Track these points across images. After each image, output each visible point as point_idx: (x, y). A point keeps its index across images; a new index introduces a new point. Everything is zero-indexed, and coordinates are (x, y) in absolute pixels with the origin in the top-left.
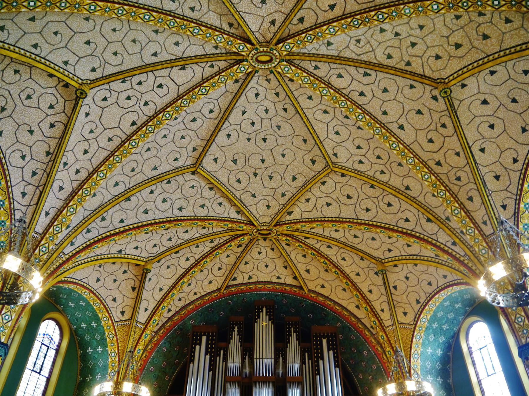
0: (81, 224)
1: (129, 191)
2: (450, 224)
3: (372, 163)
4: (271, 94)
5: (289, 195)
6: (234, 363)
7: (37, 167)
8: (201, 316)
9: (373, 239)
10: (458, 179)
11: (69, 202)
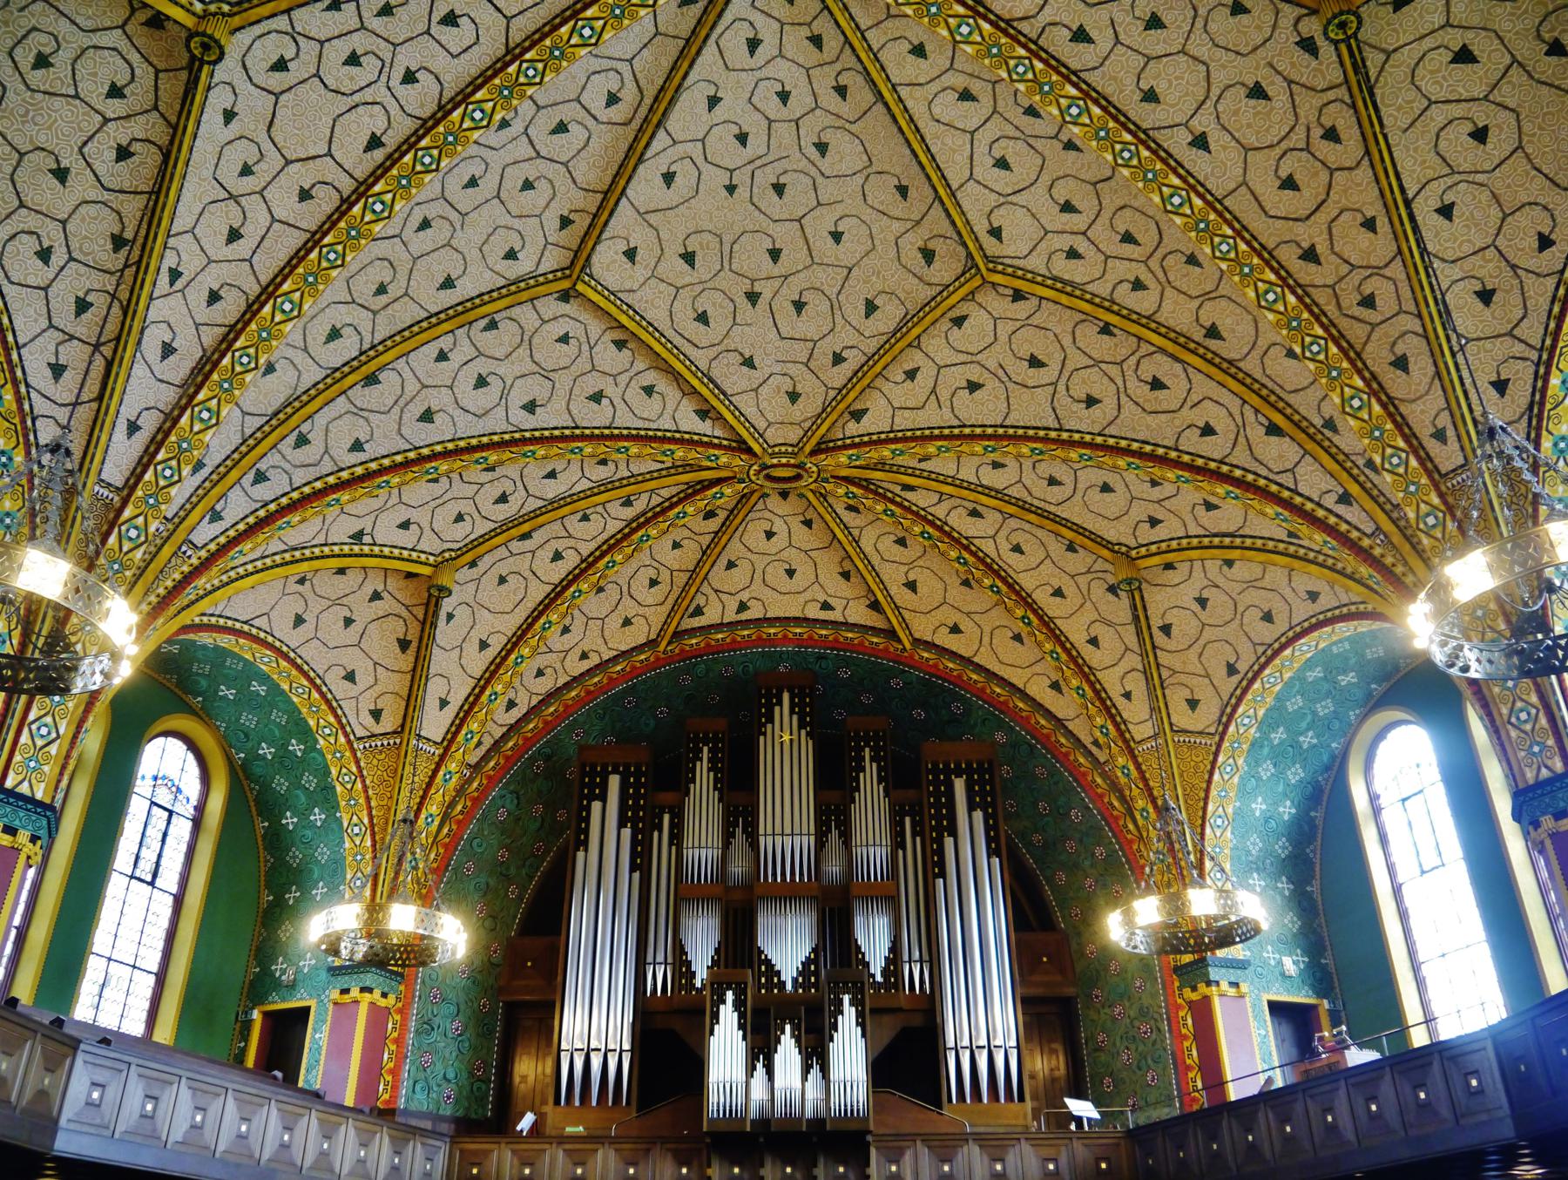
0: (236, 456)
1: (372, 353)
2: (1336, 439)
3: (1107, 257)
4: (796, 40)
5: (854, 360)
6: (703, 844)
7: (88, 285)
8: (602, 718)
9: (1106, 488)
10: (1368, 302)
11: (196, 392)
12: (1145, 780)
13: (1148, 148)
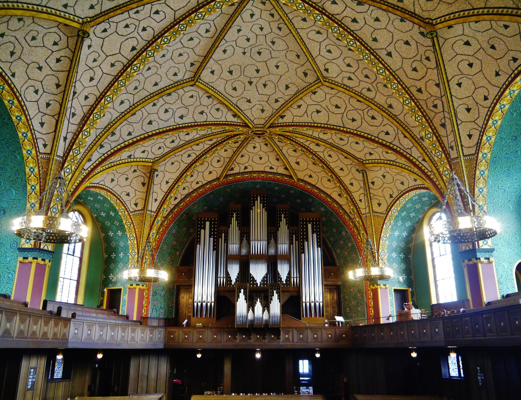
1: (133, 107)
2: (423, 143)
4: (266, 15)
5: (281, 101)
6: (234, 248)
7: (49, 99)
8: (203, 202)
10: (435, 106)
11: (83, 127)
12: (364, 226)
13: (373, 55)
